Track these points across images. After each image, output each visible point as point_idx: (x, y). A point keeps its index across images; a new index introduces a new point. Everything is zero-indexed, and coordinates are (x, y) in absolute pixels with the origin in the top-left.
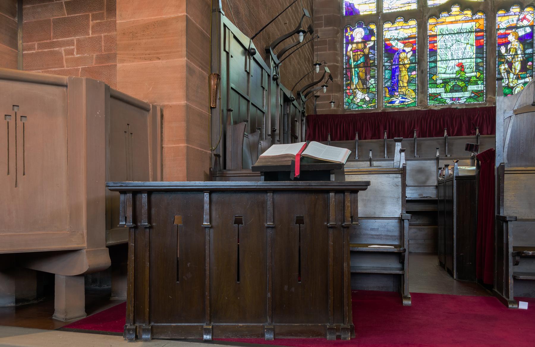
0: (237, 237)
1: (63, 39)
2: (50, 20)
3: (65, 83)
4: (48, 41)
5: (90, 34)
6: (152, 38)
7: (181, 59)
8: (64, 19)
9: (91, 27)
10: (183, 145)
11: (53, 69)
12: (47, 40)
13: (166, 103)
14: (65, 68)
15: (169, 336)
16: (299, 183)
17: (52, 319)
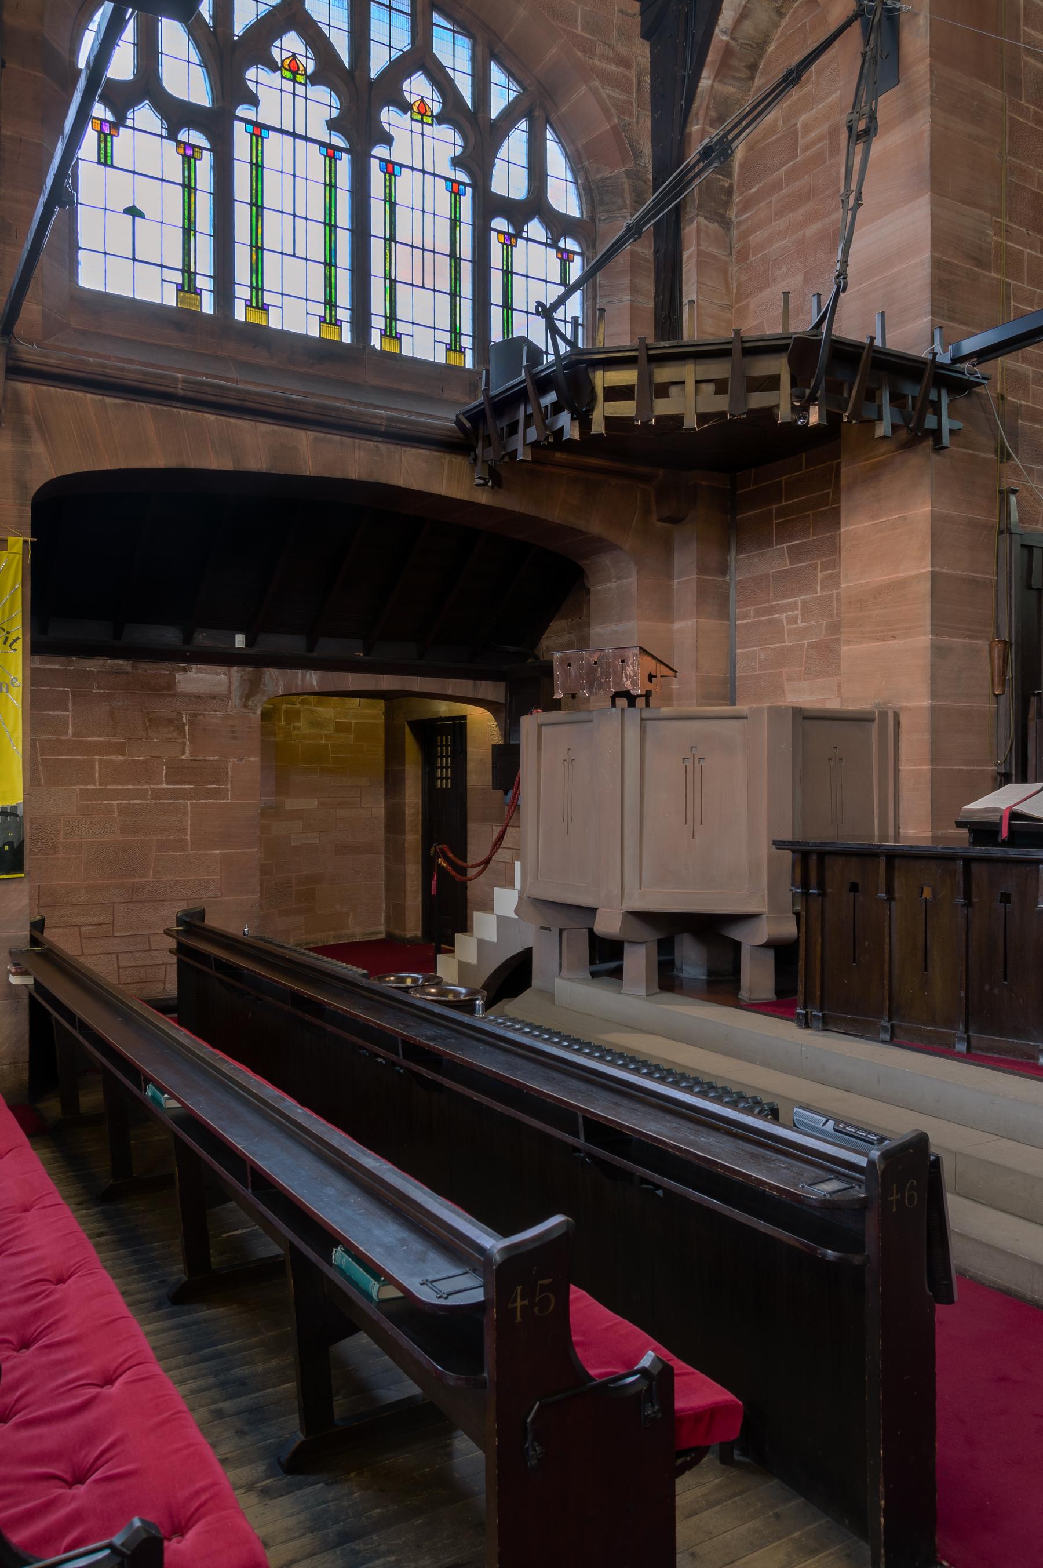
0: (924, 914)
1: (784, 601)
2: (769, 574)
3: (745, 714)
4: (766, 605)
5: (819, 592)
6: (885, 607)
7: (923, 638)
8: (786, 572)
9: (819, 581)
10: (926, 767)
11: (773, 646)
12: (765, 603)
13: (903, 704)
14: (787, 644)
15: (844, 1030)
16: (993, 850)
17: (738, 998)
